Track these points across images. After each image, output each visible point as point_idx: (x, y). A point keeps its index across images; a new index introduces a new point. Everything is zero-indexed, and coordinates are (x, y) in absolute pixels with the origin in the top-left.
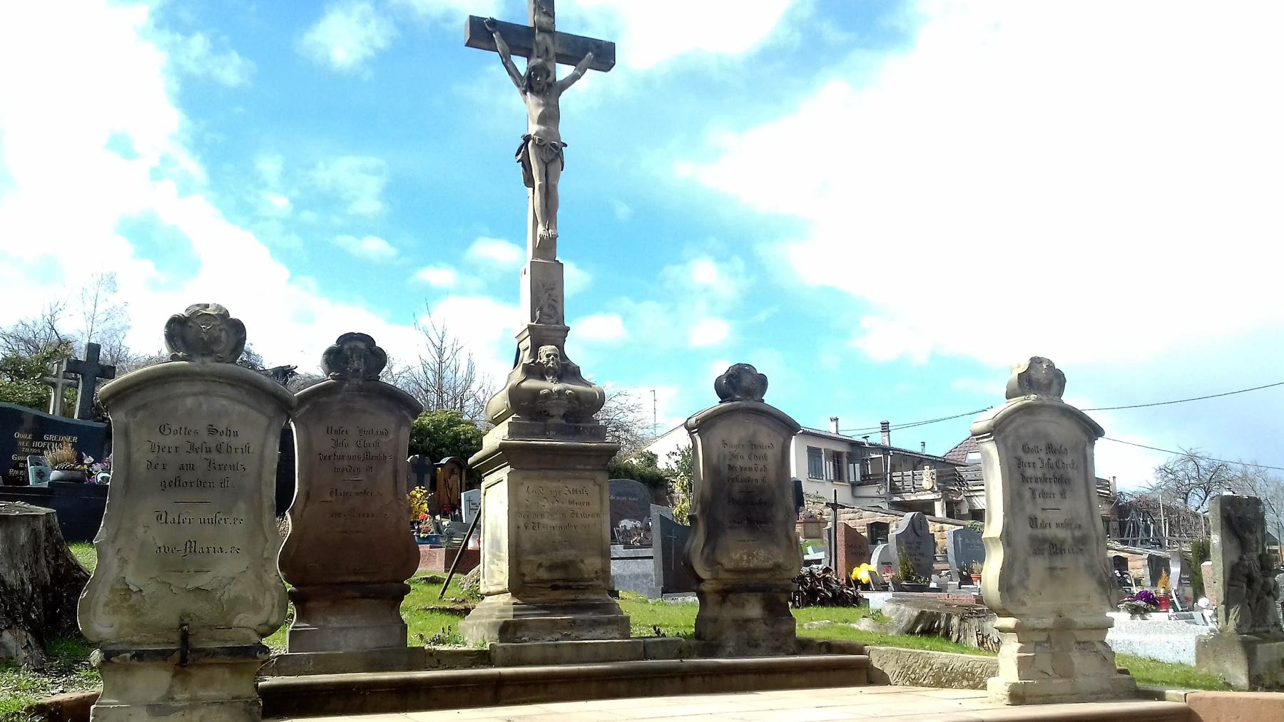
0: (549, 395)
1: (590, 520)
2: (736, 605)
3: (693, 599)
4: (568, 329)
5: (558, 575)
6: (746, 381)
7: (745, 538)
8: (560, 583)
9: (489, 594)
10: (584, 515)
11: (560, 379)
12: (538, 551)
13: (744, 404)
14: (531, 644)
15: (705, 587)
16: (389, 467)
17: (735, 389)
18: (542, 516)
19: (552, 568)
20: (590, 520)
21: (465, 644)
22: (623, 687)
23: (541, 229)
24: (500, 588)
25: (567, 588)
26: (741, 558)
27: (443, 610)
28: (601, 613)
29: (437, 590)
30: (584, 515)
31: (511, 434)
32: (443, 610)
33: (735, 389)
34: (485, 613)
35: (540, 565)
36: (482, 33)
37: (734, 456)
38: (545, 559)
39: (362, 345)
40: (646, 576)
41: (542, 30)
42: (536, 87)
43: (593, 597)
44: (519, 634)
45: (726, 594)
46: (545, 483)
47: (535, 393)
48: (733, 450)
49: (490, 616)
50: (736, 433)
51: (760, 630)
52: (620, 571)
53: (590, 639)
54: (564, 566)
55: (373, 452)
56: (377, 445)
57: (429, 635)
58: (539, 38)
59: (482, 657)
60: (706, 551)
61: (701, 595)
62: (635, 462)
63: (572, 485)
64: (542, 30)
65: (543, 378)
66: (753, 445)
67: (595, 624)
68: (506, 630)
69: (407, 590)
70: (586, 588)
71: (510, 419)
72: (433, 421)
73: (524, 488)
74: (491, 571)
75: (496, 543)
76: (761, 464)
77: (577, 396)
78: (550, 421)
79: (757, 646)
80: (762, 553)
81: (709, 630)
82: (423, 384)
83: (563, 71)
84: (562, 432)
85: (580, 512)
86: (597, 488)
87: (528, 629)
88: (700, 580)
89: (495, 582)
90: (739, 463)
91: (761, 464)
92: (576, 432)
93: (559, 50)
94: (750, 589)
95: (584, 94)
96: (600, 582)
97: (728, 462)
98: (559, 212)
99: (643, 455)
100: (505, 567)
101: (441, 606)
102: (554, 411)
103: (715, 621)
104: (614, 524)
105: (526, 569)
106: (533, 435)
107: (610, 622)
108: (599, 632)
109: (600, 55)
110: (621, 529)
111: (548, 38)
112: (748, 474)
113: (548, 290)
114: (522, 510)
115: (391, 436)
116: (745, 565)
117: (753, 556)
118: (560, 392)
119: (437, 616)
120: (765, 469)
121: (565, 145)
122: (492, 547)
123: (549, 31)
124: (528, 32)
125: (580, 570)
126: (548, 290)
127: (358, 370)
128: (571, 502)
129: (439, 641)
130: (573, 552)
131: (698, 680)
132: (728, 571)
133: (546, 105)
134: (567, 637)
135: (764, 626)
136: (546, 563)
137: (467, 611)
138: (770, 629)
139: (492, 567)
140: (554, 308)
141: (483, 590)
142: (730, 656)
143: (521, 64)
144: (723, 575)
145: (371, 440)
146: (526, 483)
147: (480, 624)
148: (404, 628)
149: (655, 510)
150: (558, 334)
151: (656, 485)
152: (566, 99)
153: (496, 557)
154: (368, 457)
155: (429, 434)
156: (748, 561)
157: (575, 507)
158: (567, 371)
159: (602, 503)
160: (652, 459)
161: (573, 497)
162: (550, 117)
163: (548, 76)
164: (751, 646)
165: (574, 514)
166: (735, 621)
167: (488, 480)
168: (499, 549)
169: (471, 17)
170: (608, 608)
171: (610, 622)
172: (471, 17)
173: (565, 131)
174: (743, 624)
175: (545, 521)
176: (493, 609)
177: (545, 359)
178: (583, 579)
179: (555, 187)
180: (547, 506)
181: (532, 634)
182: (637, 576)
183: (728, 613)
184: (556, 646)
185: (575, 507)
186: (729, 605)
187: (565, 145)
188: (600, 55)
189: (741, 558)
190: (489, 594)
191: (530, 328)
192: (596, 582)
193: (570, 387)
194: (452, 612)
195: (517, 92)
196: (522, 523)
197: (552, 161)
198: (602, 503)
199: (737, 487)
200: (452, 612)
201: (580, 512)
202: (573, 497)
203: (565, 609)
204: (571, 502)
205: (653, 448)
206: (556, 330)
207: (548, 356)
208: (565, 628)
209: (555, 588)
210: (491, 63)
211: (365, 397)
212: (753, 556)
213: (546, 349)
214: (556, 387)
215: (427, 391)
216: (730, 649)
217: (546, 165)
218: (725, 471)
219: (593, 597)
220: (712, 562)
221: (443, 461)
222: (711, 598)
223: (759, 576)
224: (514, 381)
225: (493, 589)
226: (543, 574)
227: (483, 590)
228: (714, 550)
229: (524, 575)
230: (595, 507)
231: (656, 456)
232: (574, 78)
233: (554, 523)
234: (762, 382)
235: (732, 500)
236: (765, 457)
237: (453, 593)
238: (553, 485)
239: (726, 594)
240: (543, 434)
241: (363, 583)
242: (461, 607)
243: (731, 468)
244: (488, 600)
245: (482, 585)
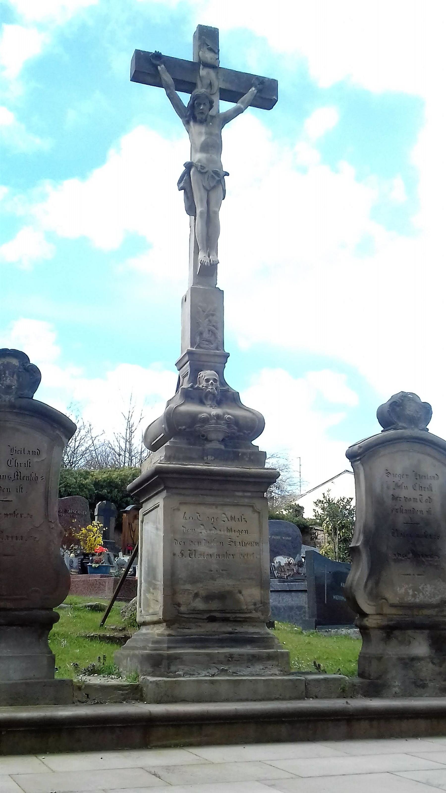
0: (206, 421)
1: (248, 549)
2: (402, 643)
3: (354, 632)
4: (227, 356)
5: (215, 605)
6: (410, 410)
7: (410, 571)
8: (217, 615)
9: (144, 624)
10: (243, 544)
11: (219, 403)
12: (194, 579)
13: (408, 432)
14: (185, 678)
15: (369, 622)
16: (41, 487)
17: (399, 418)
18: (199, 543)
19: (209, 598)
20: (248, 549)
21: (119, 675)
22: (284, 730)
23: (201, 256)
24: (155, 618)
25: (225, 620)
26: (407, 593)
27: (103, 639)
28: (259, 647)
29: (100, 616)
30: (243, 544)
31: (168, 458)
32: (103, 639)
33: (399, 418)
34: (140, 644)
35: (196, 595)
36: (148, 68)
37: (398, 486)
38: (201, 589)
39: (15, 362)
40: (300, 608)
41: (207, 65)
42: (199, 117)
43: (251, 630)
44: (173, 668)
45: (390, 630)
46: (202, 509)
47: (194, 418)
48: (397, 479)
49: (144, 648)
50: (398, 463)
51: (427, 670)
52: (275, 603)
53: (246, 674)
54: (222, 596)
55: (25, 472)
56: (28, 465)
57: (85, 664)
58: (203, 72)
59: (135, 693)
60: (370, 585)
61: (364, 631)
62: (285, 513)
63: (231, 511)
64: (207, 65)
65: (202, 402)
66: (418, 476)
67: (254, 659)
68: (158, 662)
69: (56, 618)
70: (245, 621)
71: (168, 444)
72: (120, 475)
73: (180, 514)
74: (147, 599)
75: (152, 570)
76: (426, 494)
77: (235, 422)
78: (209, 446)
79: (424, 686)
80: (429, 588)
81: (374, 669)
82: (117, 449)
83: (225, 106)
84: (220, 456)
85: (238, 540)
86: (256, 515)
87: (183, 662)
88: (364, 615)
89: (151, 611)
90: (403, 493)
91: (426, 494)
92: (235, 457)
93: (223, 86)
94: (418, 627)
95: (245, 135)
96: (259, 614)
97: (391, 492)
98: (220, 241)
99: (291, 507)
100: (160, 596)
101: (102, 633)
102: (213, 436)
103: (380, 659)
104: (272, 561)
105: (181, 599)
106: (191, 459)
107: (270, 657)
108: (258, 668)
109: (264, 93)
110: (276, 565)
111: (212, 73)
112: (413, 505)
113: (207, 316)
114: (178, 536)
115: (44, 456)
116: (410, 599)
117: (419, 591)
118: (218, 417)
119: (96, 645)
120: (430, 500)
121: (227, 174)
122: (148, 575)
123: (214, 67)
124: (193, 67)
125: (238, 602)
126: (207, 316)
127: (9, 387)
128: (230, 530)
129: (92, 671)
130: (230, 582)
131: (365, 724)
132: (393, 606)
133: (209, 134)
134: (224, 672)
135: (431, 665)
136: (203, 593)
137: (126, 638)
138: (437, 669)
139: (148, 596)
140: (214, 334)
141: (139, 619)
142: (396, 696)
143: (185, 98)
144: (387, 610)
145: (22, 460)
146: (184, 508)
147: (134, 656)
148: (52, 659)
149: (305, 549)
150: (217, 359)
151: (306, 530)
152: (229, 133)
153: (151, 584)
154: (18, 476)
155: (116, 486)
156: (414, 596)
157: (234, 535)
158: (229, 397)
159: (261, 532)
160: (299, 510)
161: (232, 524)
162: (213, 146)
163: (211, 107)
164: (418, 686)
165: (232, 542)
166: (401, 659)
167: (147, 506)
168: (155, 578)
169: (138, 53)
170: (264, 641)
171: (270, 657)
172: (138, 53)
173: (228, 160)
174: (409, 662)
175: (202, 548)
176: (147, 640)
177: (204, 384)
178: (241, 611)
179: (216, 214)
180: (204, 533)
181: (186, 669)
182: (291, 608)
183: (393, 650)
184: (212, 682)
185: (234, 535)
186: (394, 642)
187: (227, 174)
188: (264, 93)
189: (407, 593)
190: (144, 624)
191: (189, 353)
192: (254, 615)
193: (229, 412)
194: (111, 640)
195: (179, 122)
196: (178, 549)
197: (214, 188)
198: (261, 532)
199: (401, 519)
200: (111, 640)
201: (238, 540)
202: (232, 524)
203: (222, 642)
204: (230, 530)
205: (300, 502)
206: (215, 355)
207: (207, 381)
208: (221, 663)
209: (212, 619)
210: (157, 96)
211: (17, 414)
212: (419, 591)
213: (206, 374)
214: (214, 411)
215: (120, 455)
216: (397, 689)
217: (208, 191)
218: (389, 502)
219: (251, 630)
220: (375, 596)
221: (129, 508)
222: (376, 635)
223: (426, 612)
224: (173, 405)
225: (148, 618)
226: (199, 605)
227: (139, 619)
228: (377, 583)
229: (179, 605)
230: (254, 536)
231: (302, 508)
232: (238, 112)
233: (211, 551)
234: (426, 411)
235: (395, 531)
236: (430, 489)
237: (114, 621)
238: (210, 511)
239: (390, 630)
240: (201, 459)
241: (10, 609)
242: (121, 635)
243: (395, 498)
244: (144, 630)
245: (138, 614)
